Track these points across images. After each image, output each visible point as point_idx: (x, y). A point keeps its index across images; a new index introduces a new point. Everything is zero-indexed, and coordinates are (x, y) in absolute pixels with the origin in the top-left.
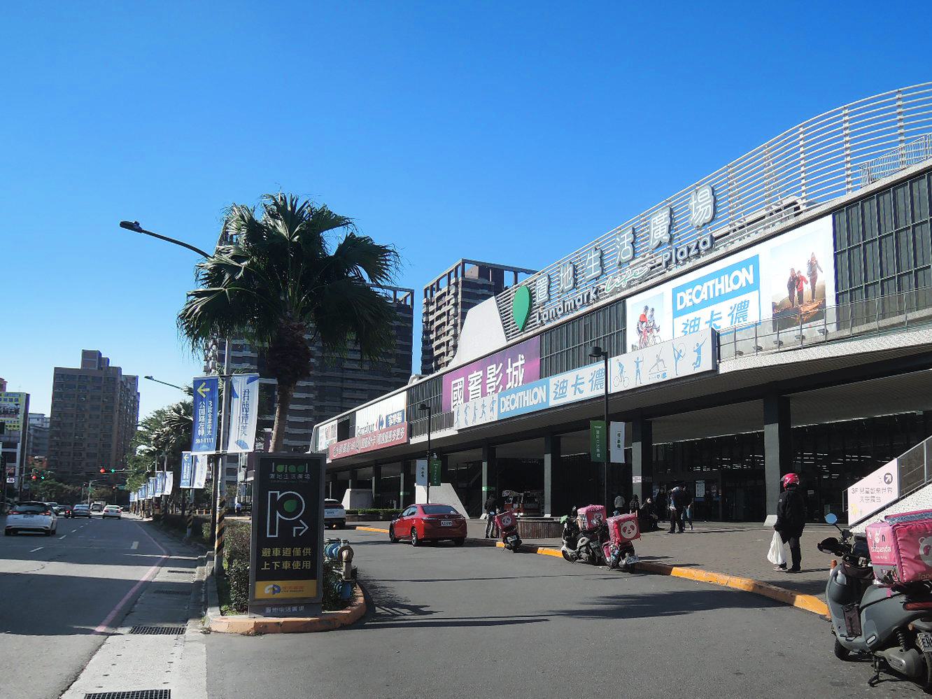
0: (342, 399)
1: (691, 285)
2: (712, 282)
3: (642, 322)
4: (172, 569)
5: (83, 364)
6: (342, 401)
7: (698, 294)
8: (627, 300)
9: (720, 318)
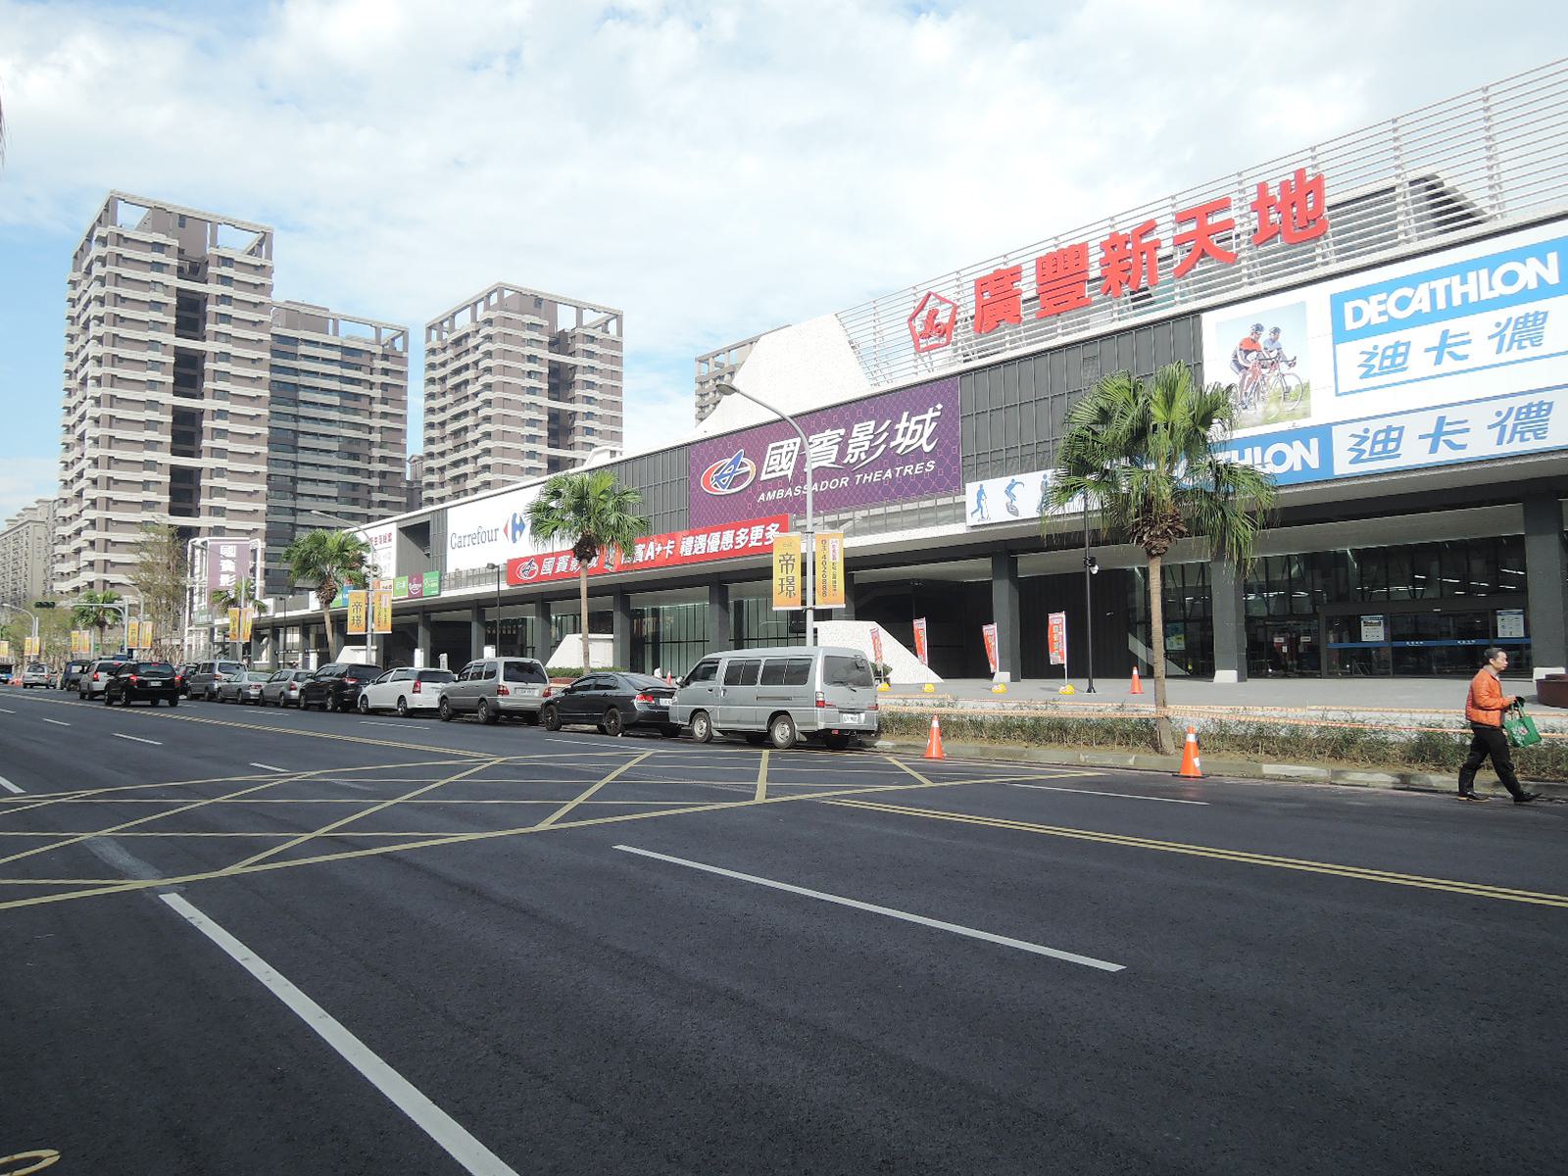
0: (296, 496)
1: (1390, 286)
2: (1446, 281)
3: (1247, 352)
4: (609, 692)
5: (1560, 279)
6: (295, 499)
7: (1403, 303)
8: (1204, 315)
9: (1469, 342)
